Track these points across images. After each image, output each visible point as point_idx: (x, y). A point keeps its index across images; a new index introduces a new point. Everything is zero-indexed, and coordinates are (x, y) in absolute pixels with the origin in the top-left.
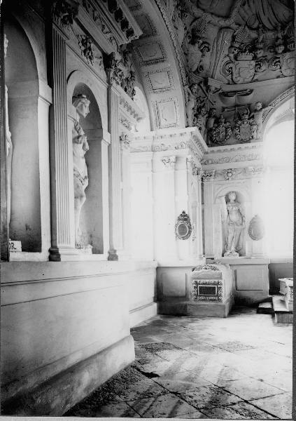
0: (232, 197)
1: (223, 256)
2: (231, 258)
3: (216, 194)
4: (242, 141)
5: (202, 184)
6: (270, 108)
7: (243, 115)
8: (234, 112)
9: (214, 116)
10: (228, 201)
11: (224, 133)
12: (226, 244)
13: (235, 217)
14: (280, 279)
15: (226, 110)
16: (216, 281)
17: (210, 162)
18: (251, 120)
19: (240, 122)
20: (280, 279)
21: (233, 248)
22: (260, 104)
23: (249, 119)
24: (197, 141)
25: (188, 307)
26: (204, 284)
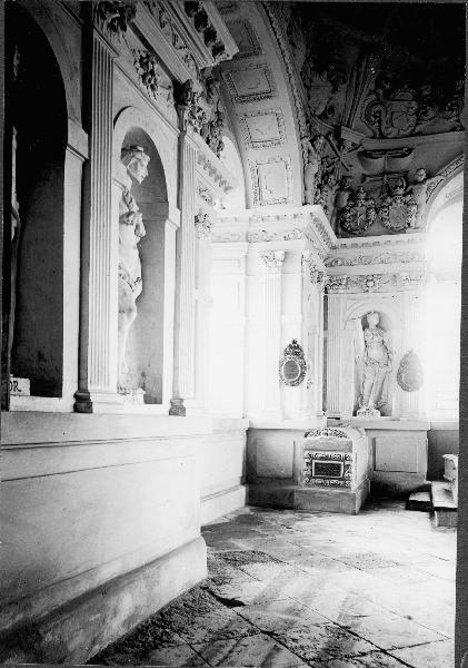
0: (373, 321)
1: (355, 414)
2: (367, 418)
3: (348, 313)
4: (392, 231)
5: (326, 298)
6: (440, 178)
7: (396, 188)
8: (380, 183)
9: (349, 189)
10: (365, 326)
11: (363, 217)
12: (360, 395)
13: (376, 353)
14: (445, 456)
15: (368, 179)
16: (343, 454)
17: (340, 262)
18: (408, 198)
19: (389, 200)
20: (445, 456)
21: (371, 403)
22: (423, 172)
23: (405, 195)
24: (321, 227)
25: (296, 495)
26: (322, 458)
